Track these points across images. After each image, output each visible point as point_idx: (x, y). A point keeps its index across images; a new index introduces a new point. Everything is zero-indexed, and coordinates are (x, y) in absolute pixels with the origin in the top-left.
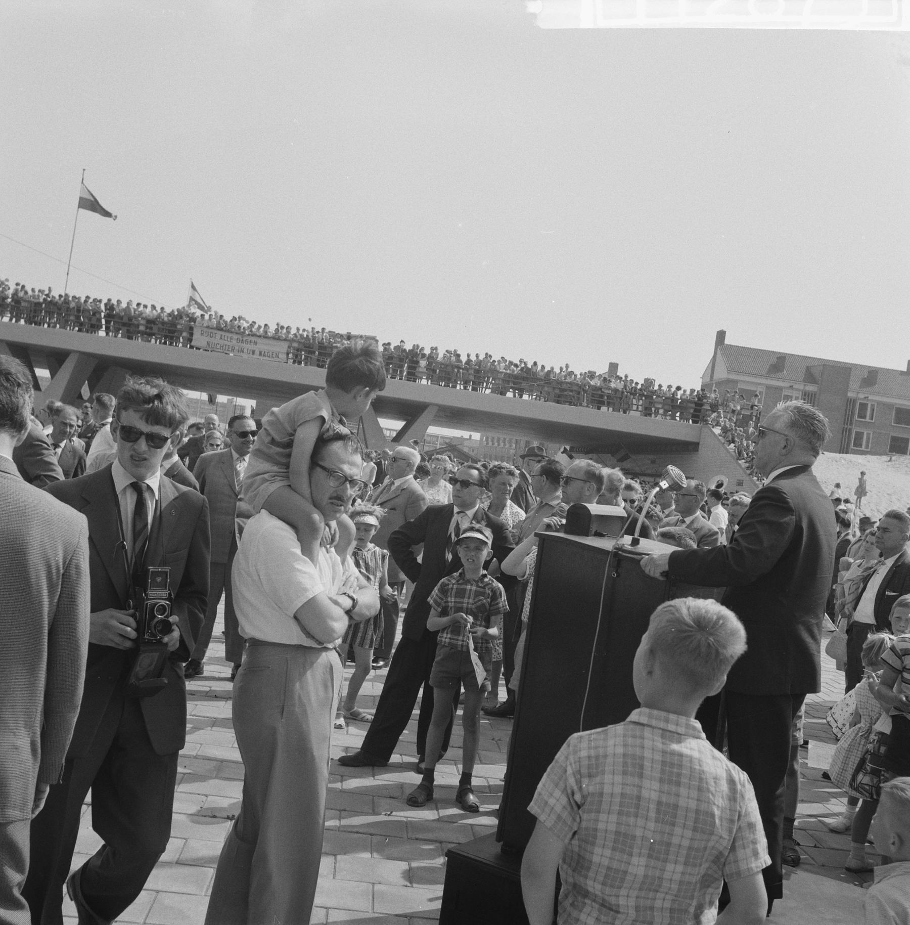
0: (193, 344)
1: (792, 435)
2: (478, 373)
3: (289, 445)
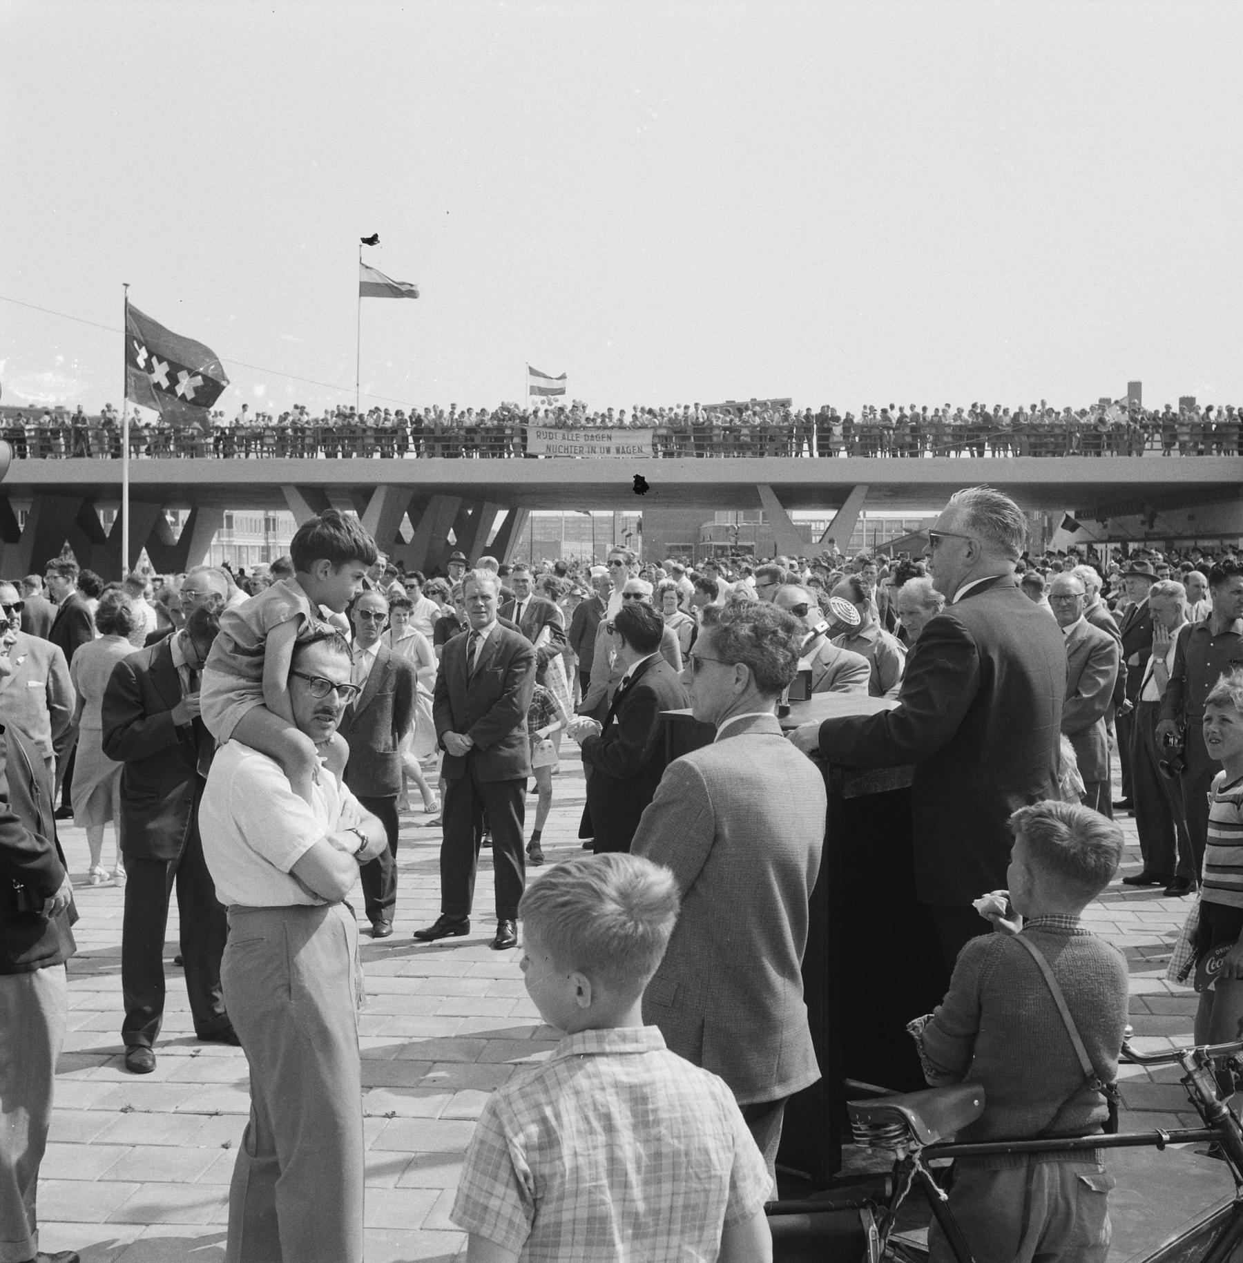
0: (528, 451)
1: (976, 536)
2: (910, 434)
3: (261, 652)
